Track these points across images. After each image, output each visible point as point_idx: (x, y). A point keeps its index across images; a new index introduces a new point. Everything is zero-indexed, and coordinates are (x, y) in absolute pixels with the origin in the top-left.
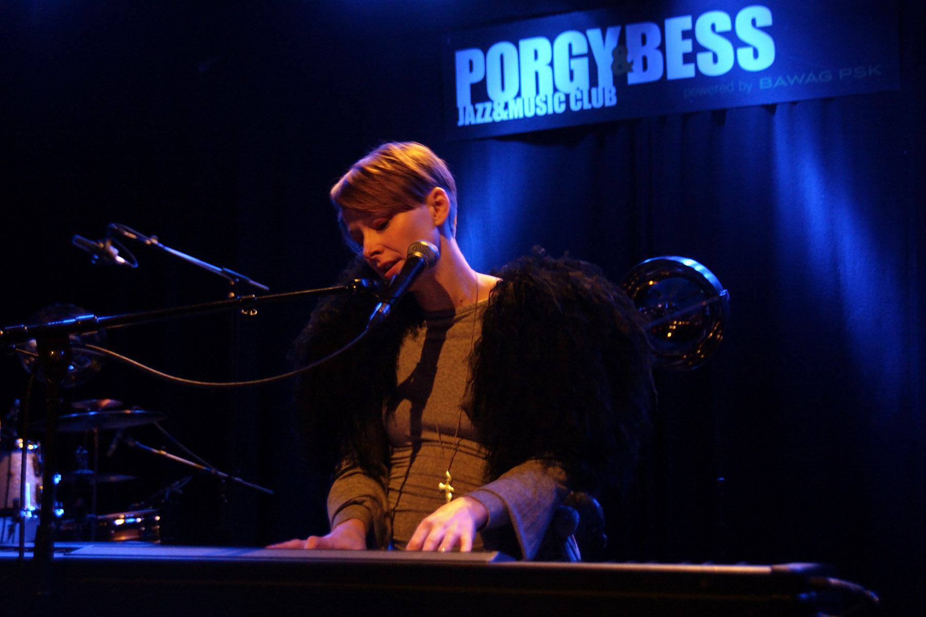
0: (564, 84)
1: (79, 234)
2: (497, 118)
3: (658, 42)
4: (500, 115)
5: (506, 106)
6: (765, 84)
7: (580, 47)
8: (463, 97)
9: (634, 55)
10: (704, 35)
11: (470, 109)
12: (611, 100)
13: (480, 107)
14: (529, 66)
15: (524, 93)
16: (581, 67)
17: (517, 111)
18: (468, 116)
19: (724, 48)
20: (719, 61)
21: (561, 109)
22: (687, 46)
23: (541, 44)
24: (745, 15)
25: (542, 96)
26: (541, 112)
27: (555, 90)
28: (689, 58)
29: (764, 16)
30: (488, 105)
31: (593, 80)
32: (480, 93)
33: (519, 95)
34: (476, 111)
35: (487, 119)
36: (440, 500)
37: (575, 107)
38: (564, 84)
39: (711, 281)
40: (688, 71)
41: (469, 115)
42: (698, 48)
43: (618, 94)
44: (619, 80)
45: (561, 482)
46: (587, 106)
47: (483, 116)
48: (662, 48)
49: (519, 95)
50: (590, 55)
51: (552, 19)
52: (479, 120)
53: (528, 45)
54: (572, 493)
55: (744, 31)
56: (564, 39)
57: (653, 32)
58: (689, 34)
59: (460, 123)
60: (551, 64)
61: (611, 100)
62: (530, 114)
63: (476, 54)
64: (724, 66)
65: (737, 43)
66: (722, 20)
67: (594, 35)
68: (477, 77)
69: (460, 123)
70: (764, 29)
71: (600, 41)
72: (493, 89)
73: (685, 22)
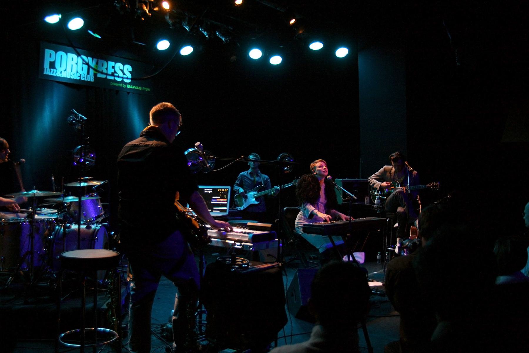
2: (58, 76)
3: (106, 67)
4: (59, 75)
5: (61, 73)
8: (47, 65)
11: (49, 69)
12: (92, 80)
13: (52, 70)
14: (70, 63)
15: (67, 70)
16: (85, 67)
21: (78, 78)
22: (113, 71)
25: (73, 73)
26: (72, 78)
27: (77, 72)
30: (55, 70)
32: (52, 65)
33: (66, 70)
34: (50, 71)
35: (54, 75)
36: (203, 346)
37: (82, 79)
41: (48, 71)
42: (115, 72)
43: (94, 79)
46: (86, 80)
47: (53, 73)
49: (66, 70)
51: (67, 47)
52: (51, 74)
54: (83, 227)
57: (105, 63)
58: (113, 67)
59: (45, 73)
60: (77, 64)
61: (92, 80)
62: (69, 77)
63: (53, 52)
68: (52, 60)
69: (45, 73)
70: (130, 72)
72: (57, 65)
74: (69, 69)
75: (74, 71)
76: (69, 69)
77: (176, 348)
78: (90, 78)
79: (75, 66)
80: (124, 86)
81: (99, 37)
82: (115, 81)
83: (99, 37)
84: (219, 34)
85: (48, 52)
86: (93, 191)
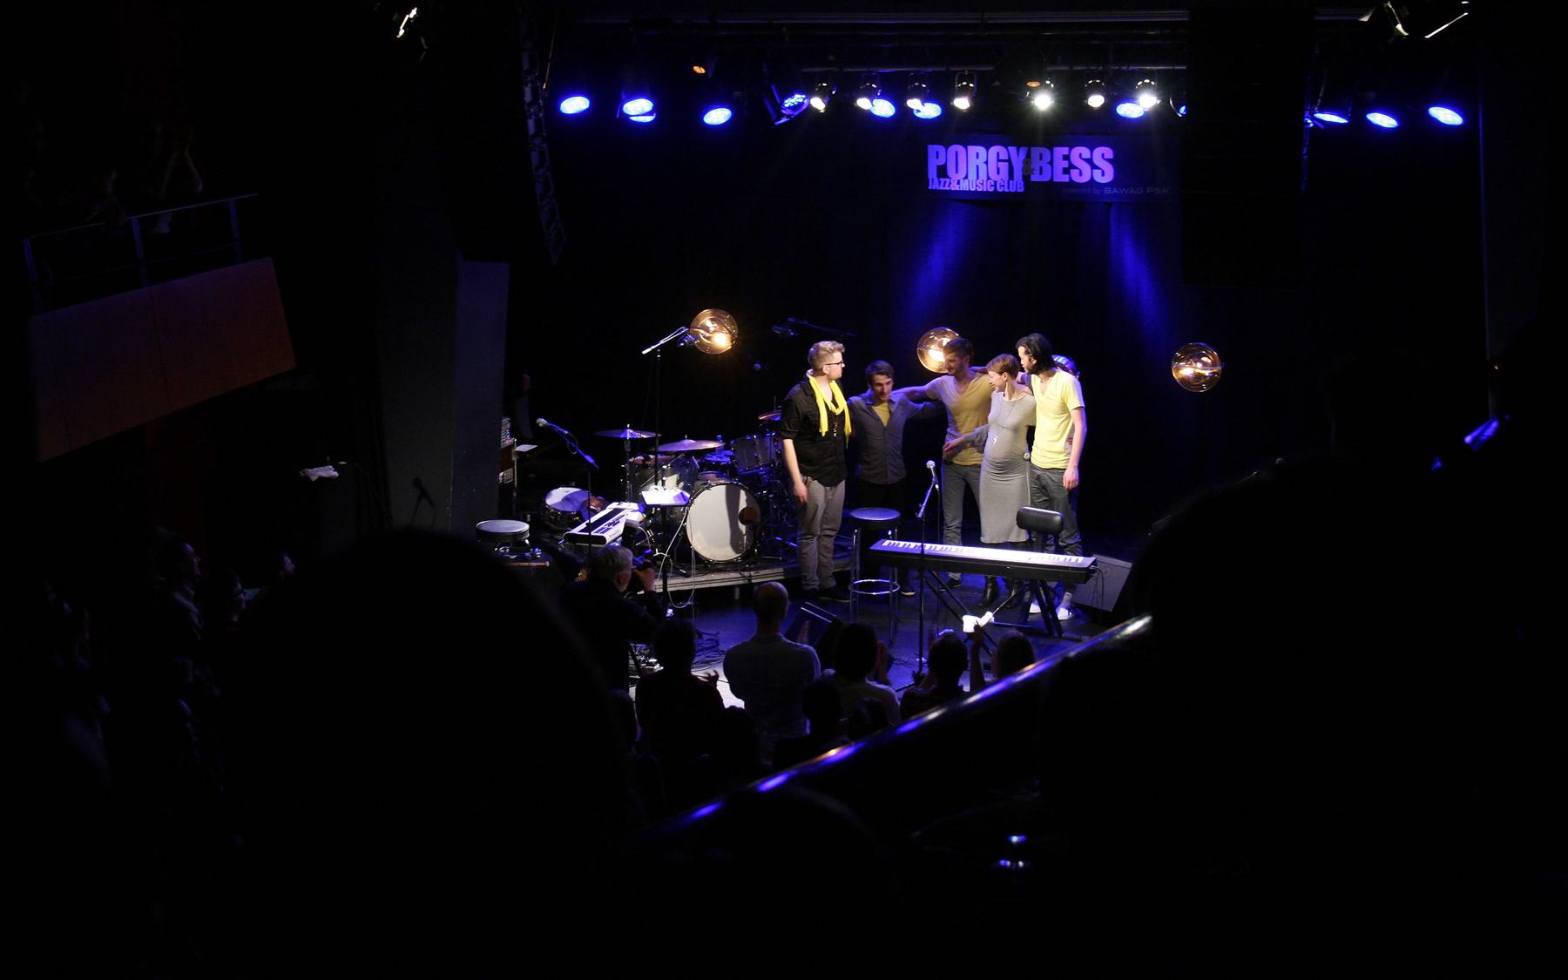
0: (994, 176)
1: (1497, 429)
6: (1107, 191)
7: (1004, 156)
8: (932, 173)
9: (1036, 164)
10: (1075, 160)
14: (973, 162)
16: (1004, 167)
17: (964, 186)
18: (935, 184)
19: (1086, 168)
20: (1083, 175)
22: (1065, 164)
23: (981, 150)
24: (1098, 151)
28: (1066, 171)
29: (1109, 153)
31: (1011, 176)
32: (942, 172)
36: (248, 602)
38: (994, 176)
39: (1041, 668)
40: (1065, 179)
42: (1072, 166)
44: (1026, 178)
45: (1013, 369)
48: (1051, 163)
50: (1009, 161)
53: (973, 149)
55: (1098, 161)
56: (994, 150)
58: (1066, 158)
63: (941, 149)
64: (1086, 178)
65: (1094, 167)
66: (1086, 152)
67: (1012, 149)
68: (941, 162)
71: (1018, 158)
73: (1065, 150)
74: (972, 176)
75: (983, 176)
76: (972, 176)
77: (307, 478)
78: (1018, 186)
79: (983, 168)
80: (1097, 192)
81: (1342, 121)
82: (1072, 183)
83: (1342, 121)
84: (807, 112)
85: (932, 149)
86: (579, 514)
